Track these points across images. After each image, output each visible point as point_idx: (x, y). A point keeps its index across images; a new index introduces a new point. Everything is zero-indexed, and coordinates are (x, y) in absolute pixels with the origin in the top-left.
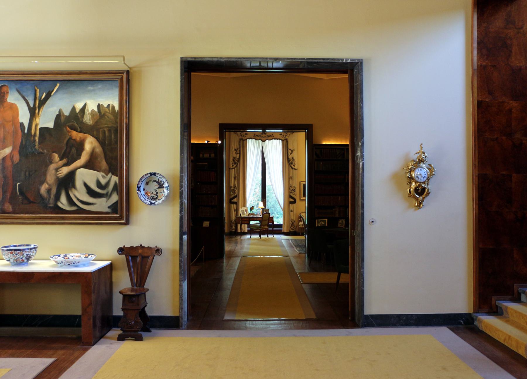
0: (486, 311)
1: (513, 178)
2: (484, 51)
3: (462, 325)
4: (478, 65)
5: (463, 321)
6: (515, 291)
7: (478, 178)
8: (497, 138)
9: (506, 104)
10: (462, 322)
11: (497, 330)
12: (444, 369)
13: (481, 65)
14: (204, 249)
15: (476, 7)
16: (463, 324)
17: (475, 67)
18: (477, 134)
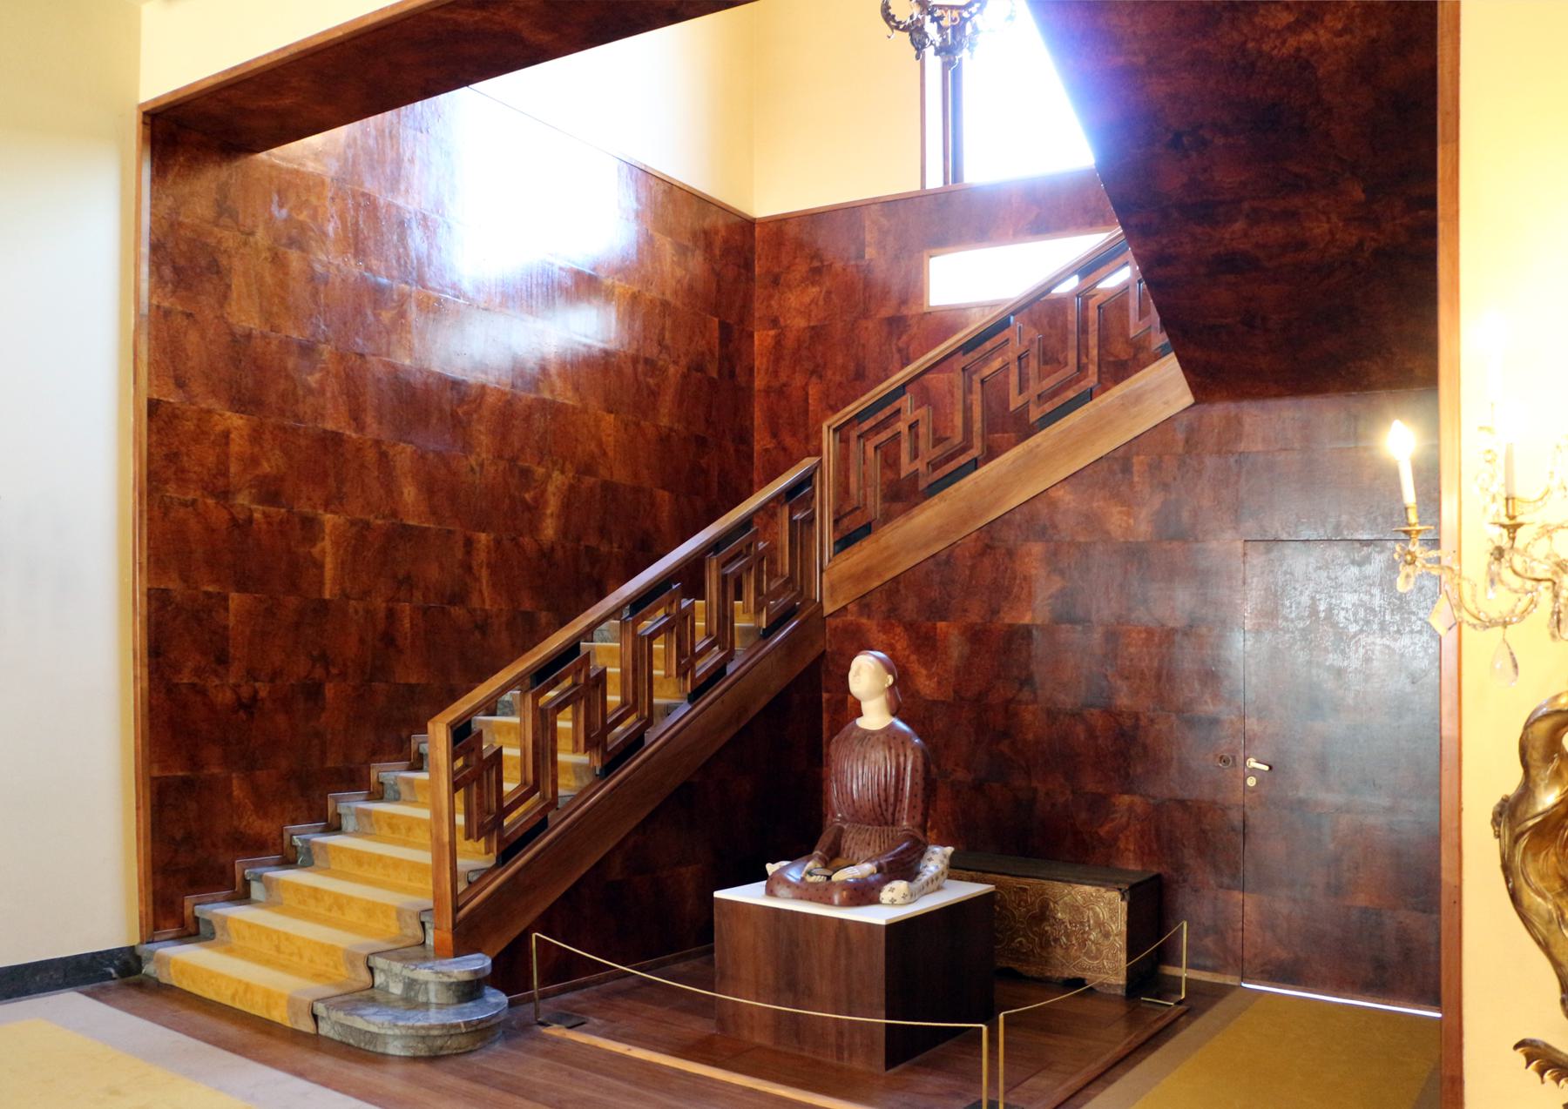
0: (170, 935)
1: (230, 601)
2: (167, 272)
3: (115, 979)
4: (150, 305)
5: (114, 968)
6: (238, 878)
7: (149, 597)
8: (194, 502)
9: (217, 417)
10: (112, 971)
11: (212, 976)
12: (114, 1092)
13: (158, 307)
14: (681, 967)
15: (149, 148)
16: (114, 975)
17: (145, 310)
18: (145, 484)
